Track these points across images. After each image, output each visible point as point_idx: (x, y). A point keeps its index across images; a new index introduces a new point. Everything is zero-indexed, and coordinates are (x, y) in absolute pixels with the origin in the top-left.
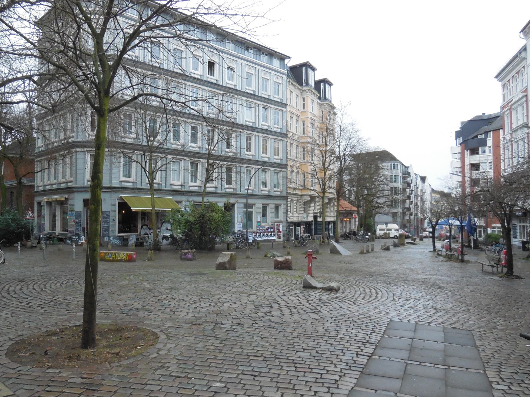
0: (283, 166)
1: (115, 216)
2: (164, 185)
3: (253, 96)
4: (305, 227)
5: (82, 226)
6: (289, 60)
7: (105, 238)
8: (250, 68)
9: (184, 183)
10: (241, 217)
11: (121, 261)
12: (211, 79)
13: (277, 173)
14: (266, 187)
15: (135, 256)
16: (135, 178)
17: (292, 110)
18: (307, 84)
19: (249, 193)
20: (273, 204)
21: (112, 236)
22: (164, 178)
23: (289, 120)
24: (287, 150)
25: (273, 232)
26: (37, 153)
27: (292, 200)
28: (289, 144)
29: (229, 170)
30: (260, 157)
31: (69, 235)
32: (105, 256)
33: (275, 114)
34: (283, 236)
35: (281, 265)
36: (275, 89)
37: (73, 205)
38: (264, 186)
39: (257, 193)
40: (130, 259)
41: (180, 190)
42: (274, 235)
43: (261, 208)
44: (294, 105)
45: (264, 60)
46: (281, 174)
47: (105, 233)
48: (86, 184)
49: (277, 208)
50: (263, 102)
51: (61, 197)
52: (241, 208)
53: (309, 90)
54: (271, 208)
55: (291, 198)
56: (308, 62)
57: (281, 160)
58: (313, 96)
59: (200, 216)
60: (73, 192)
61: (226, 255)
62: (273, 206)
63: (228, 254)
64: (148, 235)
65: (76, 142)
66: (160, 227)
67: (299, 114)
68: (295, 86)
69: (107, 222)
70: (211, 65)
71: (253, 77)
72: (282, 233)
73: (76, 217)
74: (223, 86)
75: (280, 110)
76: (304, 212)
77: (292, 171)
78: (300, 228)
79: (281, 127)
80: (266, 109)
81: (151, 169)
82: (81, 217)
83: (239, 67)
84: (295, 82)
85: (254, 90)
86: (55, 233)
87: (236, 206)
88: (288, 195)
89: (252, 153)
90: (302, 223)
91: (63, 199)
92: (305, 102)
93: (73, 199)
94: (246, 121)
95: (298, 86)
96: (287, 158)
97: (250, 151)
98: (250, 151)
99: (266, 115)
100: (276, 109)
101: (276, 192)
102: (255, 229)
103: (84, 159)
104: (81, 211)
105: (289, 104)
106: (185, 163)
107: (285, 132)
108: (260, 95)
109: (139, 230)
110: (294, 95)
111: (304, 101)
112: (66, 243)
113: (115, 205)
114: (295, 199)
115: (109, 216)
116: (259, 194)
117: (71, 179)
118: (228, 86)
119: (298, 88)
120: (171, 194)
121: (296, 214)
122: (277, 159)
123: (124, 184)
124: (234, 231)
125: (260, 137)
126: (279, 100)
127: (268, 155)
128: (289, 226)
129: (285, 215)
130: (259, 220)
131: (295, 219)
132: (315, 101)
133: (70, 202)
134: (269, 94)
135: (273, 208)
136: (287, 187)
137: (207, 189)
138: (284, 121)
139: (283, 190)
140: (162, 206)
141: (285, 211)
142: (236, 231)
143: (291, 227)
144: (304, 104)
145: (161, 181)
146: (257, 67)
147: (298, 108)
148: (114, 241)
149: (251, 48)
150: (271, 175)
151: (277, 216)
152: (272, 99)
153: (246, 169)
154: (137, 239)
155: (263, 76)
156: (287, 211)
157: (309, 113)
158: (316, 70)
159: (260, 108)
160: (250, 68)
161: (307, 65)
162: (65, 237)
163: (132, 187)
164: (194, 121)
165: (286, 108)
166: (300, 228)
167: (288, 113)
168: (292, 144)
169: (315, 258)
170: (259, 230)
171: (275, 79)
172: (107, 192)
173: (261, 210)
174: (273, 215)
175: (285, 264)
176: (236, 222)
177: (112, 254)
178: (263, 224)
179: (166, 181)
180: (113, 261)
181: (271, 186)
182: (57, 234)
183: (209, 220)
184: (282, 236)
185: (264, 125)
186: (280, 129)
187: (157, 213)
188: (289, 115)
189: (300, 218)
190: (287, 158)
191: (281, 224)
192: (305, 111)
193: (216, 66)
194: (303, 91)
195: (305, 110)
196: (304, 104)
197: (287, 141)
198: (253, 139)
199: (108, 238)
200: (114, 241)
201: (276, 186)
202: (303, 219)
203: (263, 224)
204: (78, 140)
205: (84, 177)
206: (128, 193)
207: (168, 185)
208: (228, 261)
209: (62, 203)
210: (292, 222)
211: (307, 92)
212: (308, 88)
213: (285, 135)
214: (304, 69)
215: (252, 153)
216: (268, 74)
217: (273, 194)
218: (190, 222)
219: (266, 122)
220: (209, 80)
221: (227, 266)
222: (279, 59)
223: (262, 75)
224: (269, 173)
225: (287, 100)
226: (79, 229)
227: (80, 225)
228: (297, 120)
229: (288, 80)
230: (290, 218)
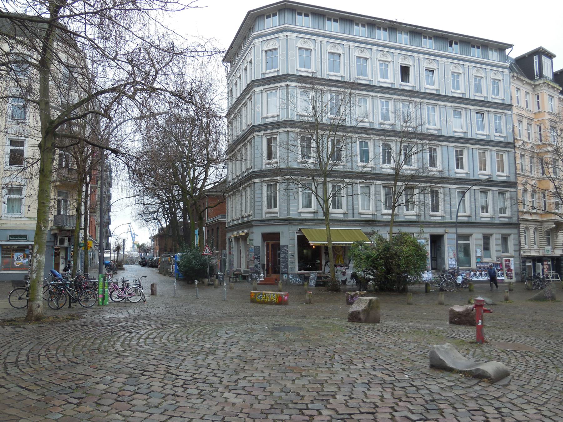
0: (513, 185)
1: (294, 250)
2: (350, 214)
3: (463, 100)
4: (550, 263)
6: (511, 49)
7: (284, 276)
8: (496, 74)
9: (376, 211)
10: (453, 251)
11: (271, 303)
12: (407, 86)
13: (502, 194)
14: (487, 212)
15: (286, 298)
16: (374, 210)
17: (520, 112)
18: (541, 75)
19: (458, 221)
20: (499, 234)
21: (291, 274)
22: (473, 210)
23: (516, 124)
24: (515, 163)
25: (500, 270)
26: (228, 187)
27: (527, 228)
28: (518, 156)
29: (435, 193)
30: (476, 174)
32: (255, 297)
33: (496, 119)
34: (516, 275)
35: (459, 318)
36: (493, 87)
38: (485, 211)
39: (474, 221)
40: (281, 302)
41: (372, 219)
42: (503, 274)
43: (481, 239)
44: (523, 104)
45: (476, 53)
46: (508, 195)
47: (284, 270)
48: (264, 217)
49: (505, 239)
50: (477, 105)
51: (242, 233)
52: (452, 239)
53: (544, 83)
54: (496, 239)
55: (525, 226)
56: (541, 47)
57: (507, 176)
58: (551, 90)
59: (385, 250)
60: (252, 226)
61: (362, 301)
62: (499, 236)
63: (365, 300)
65: (254, 172)
66: (347, 263)
67: (532, 116)
68: (522, 81)
69: (286, 258)
70: (405, 71)
71: (461, 78)
72: (513, 272)
74: (323, 79)
75: (502, 113)
76: (549, 244)
77: (525, 190)
78: (543, 264)
79: (505, 135)
80: (482, 114)
81: (325, 196)
82: (259, 253)
83: (441, 67)
84: (522, 75)
85: (463, 92)
86: (240, 271)
87: (446, 237)
88: (520, 222)
89: (465, 170)
90: (544, 258)
91: (244, 234)
92: (540, 100)
93: (252, 233)
94: (454, 132)
95: (527, 80)
96: (516, 174)
97: (462, 168)
98: (462, 168)
99: (483, 122)
100: (495, 113)
101: (504, 217)
102: (474, 266)
105: (515, 104)
106: (375, 188)
107: (512, 141)
108: (472, 97)
109: (323, 267)
110: (522, 93)
111: (538, 99)
112: (248, 280)
113: (294, 239)
114: (532, 227)
116: (478, 221)
117: (251, 212)
118: (428, 91)
119: (527, 83)
120: (360, 225)
121: (536, 247)
122: (501, 176)
123: (304, 216)
124: (444, 269)
125: (475, 151)
126: (500, 102)
127: (488, 171)
128: (524, 262)
129: (517, 248)
130: (479, 254)
131: (533, 253)
132: (555, 96)
133: (250, 237)
134: (485, 95)
135: (499, 239)
136: (518, 212)
137: (459, 218)
138: (510, 126)
139: (512, 215)
140: (347, 240)
141: (517, 242)
142: (447, 268)
143: (527, 264)
144: (538, 102)
145: (347, 210)
146: (466, 64)
147: (530, 107)
148: (294, 279)
149: (456, 43)
150: (493, 197)
151: (506, 249)
152: (490, 100)
153: (457, 191)
154: (318, 278)
155: (474, 75)
156: (520, 242)
157: (546, 114)
158: (555, 56)
159: (474, 114)
160: (496, 74)
161: (540, 53)
163: (313, 218)
164: (363, 135)
165: (510, 110)
166: (543, 264)
167: (514, 116)
168: (522, 156)
169: (489, 311)
170: (480, 268)
171: (492, 75)
173: (481, 242)
174: (500, 248)
175: (465, 316)
176: (446, 257)
177: (262, 294)
178: (485, 260)
179: (353, 210)
180: (263, 303)
181: (494, 210)
182: (242, 272)
183: (395, 254)
184: (513, 275)
185: (481, 134)
186: (504, 137)
187: (334, 247)
188: (516, 118)
189: (541, 251)
190: (516, 174)
191: (512, 259)
192: (541, 112)
193: (411, 70)
194: (535, 86)
195: (541, 110)
196: (538, 102)
197: (515, 153)
198: (465, 153)
199: (286, 275)
200: (294, 279)
201: (503, 211)
202: (546, 253)
203: (485, 260)
204: (256, 170)
205: (262, 209)
206: (309, 225)
207: (356, 214)
208: (364, 310)
209: (245, 238)
210: (528, 258)
211: (541, 87)
212: (542, 81)
213: (512, 145)
214: (536, 59)
215: (465, 170)
216: (499, 74)
217: (497, 221)
218: (371, 257)
219: (483, 130)
220: (402, 88)
221: (362, 316)
222: (496, 51)
223: (474, 72)
224: (490, 194)
225: (511, 100)
226: (259, 266)
227: (259, 262)
228: (529, 125)
229: (511, 74)
230: (525, 252)
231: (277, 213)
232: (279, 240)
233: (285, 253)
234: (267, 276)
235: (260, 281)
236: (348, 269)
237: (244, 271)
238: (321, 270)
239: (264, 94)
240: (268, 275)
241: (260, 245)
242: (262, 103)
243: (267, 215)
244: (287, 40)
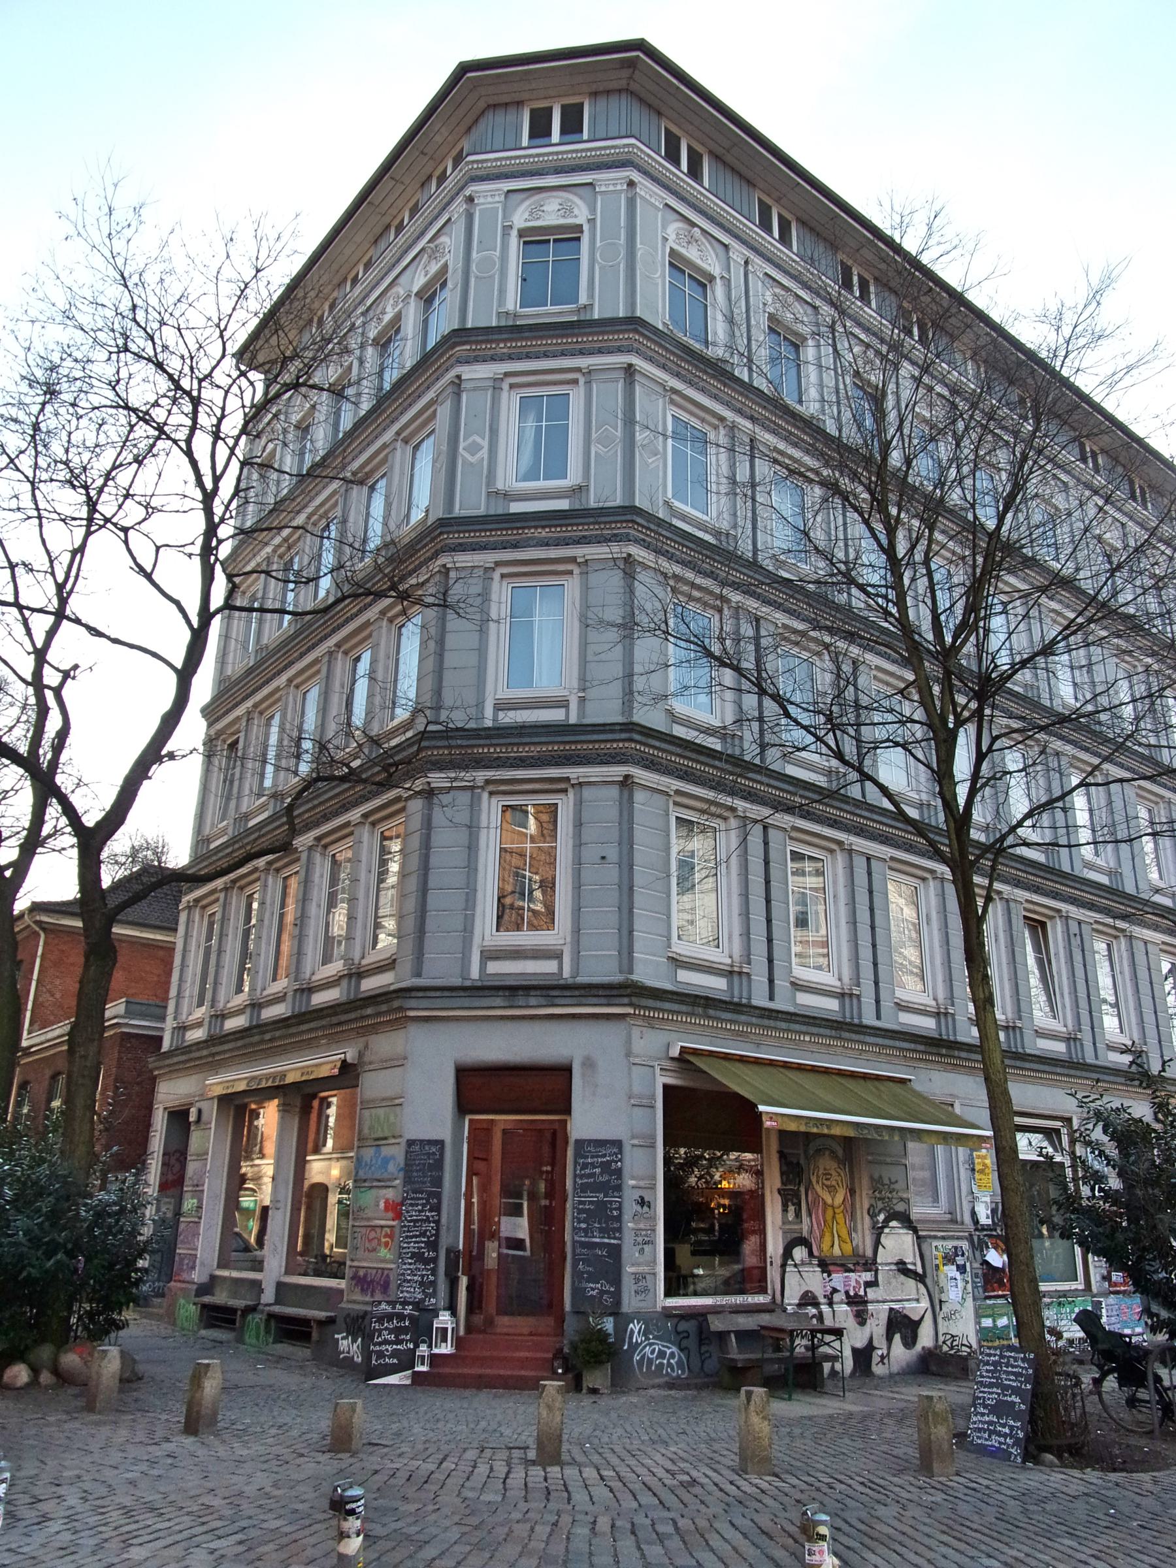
5: (445, 1242)
31: (356, 1301)
37: (394, 1103)
48: (475, 973)
64: (816, 1304)
73: (408, 1180)
82: (438, 1182)
86: (257, 1285)
93: (397, 1062)
103: (473, 829)
104: (440, 1143)
109: (773, 1274)
115: (619, 1173)
162: (322, 1315)
172: (574, 1016)
205: (468, 930)
207: (886, 1004)
231: (558, 956)
232: (568, 1111)
233: (604, 1188)
234: (469, 1329)
235: (435, 1359)
236: (873, 1284)
237: (280, 1286)
238: (763, 1290)
239: (505, 395)
240: (478, 1319)
241: (444, 1132)
242: (494, 432)
243: (494, 967)
244: (631, 203)
